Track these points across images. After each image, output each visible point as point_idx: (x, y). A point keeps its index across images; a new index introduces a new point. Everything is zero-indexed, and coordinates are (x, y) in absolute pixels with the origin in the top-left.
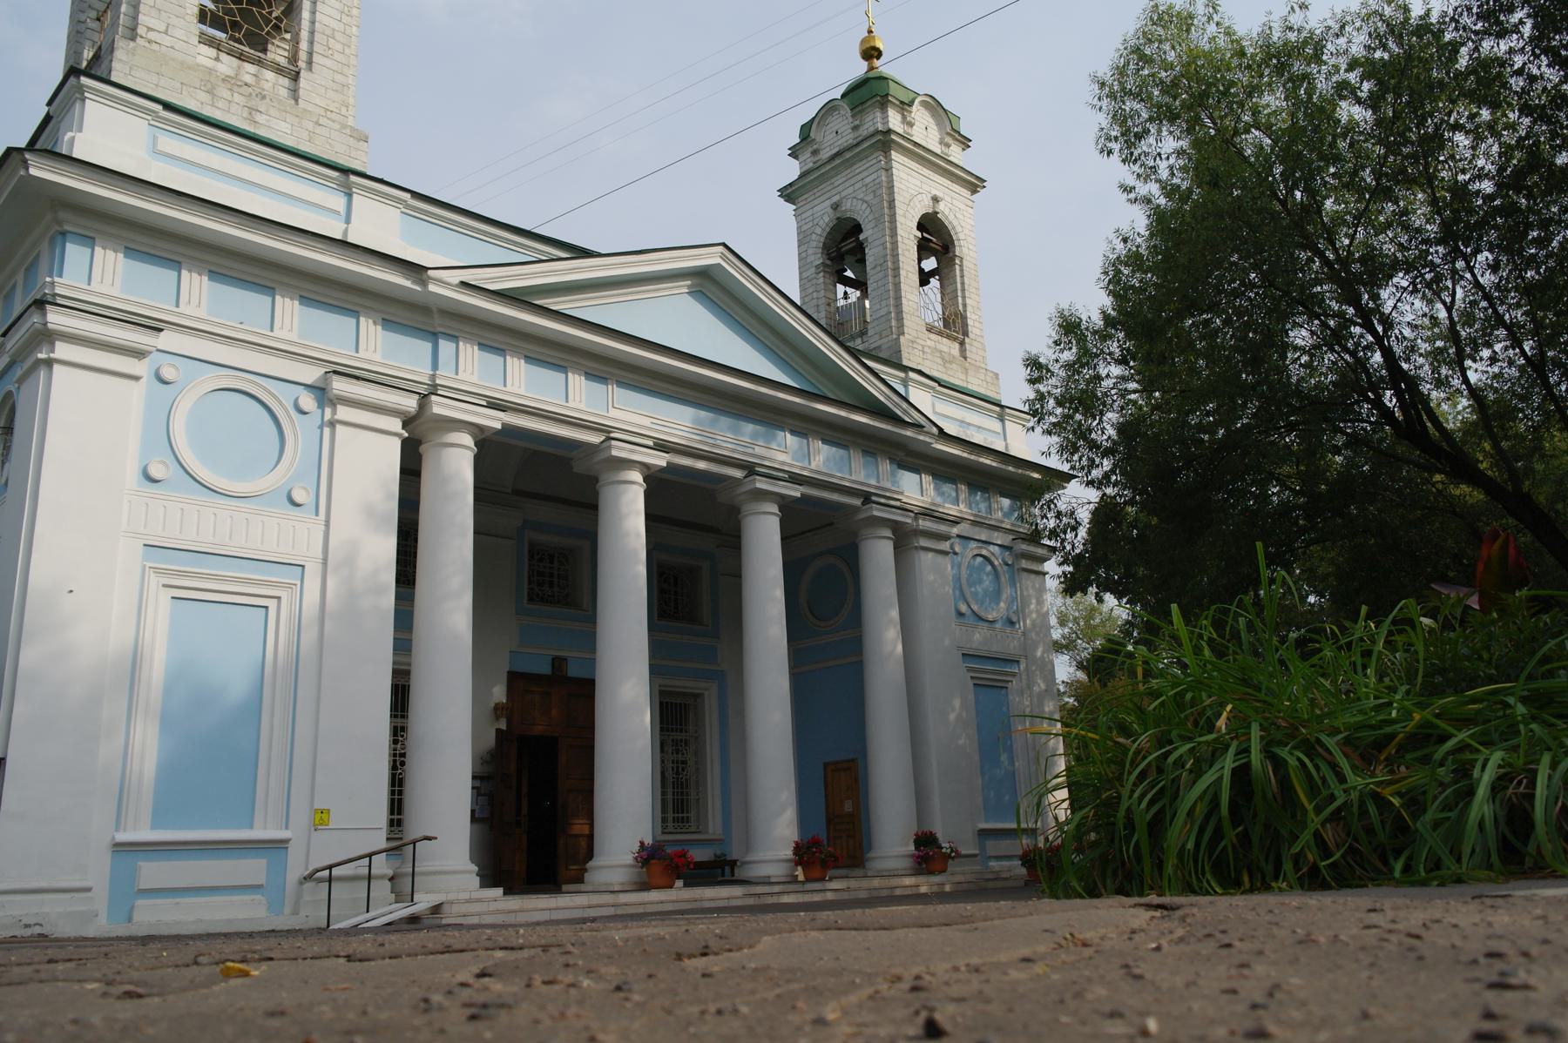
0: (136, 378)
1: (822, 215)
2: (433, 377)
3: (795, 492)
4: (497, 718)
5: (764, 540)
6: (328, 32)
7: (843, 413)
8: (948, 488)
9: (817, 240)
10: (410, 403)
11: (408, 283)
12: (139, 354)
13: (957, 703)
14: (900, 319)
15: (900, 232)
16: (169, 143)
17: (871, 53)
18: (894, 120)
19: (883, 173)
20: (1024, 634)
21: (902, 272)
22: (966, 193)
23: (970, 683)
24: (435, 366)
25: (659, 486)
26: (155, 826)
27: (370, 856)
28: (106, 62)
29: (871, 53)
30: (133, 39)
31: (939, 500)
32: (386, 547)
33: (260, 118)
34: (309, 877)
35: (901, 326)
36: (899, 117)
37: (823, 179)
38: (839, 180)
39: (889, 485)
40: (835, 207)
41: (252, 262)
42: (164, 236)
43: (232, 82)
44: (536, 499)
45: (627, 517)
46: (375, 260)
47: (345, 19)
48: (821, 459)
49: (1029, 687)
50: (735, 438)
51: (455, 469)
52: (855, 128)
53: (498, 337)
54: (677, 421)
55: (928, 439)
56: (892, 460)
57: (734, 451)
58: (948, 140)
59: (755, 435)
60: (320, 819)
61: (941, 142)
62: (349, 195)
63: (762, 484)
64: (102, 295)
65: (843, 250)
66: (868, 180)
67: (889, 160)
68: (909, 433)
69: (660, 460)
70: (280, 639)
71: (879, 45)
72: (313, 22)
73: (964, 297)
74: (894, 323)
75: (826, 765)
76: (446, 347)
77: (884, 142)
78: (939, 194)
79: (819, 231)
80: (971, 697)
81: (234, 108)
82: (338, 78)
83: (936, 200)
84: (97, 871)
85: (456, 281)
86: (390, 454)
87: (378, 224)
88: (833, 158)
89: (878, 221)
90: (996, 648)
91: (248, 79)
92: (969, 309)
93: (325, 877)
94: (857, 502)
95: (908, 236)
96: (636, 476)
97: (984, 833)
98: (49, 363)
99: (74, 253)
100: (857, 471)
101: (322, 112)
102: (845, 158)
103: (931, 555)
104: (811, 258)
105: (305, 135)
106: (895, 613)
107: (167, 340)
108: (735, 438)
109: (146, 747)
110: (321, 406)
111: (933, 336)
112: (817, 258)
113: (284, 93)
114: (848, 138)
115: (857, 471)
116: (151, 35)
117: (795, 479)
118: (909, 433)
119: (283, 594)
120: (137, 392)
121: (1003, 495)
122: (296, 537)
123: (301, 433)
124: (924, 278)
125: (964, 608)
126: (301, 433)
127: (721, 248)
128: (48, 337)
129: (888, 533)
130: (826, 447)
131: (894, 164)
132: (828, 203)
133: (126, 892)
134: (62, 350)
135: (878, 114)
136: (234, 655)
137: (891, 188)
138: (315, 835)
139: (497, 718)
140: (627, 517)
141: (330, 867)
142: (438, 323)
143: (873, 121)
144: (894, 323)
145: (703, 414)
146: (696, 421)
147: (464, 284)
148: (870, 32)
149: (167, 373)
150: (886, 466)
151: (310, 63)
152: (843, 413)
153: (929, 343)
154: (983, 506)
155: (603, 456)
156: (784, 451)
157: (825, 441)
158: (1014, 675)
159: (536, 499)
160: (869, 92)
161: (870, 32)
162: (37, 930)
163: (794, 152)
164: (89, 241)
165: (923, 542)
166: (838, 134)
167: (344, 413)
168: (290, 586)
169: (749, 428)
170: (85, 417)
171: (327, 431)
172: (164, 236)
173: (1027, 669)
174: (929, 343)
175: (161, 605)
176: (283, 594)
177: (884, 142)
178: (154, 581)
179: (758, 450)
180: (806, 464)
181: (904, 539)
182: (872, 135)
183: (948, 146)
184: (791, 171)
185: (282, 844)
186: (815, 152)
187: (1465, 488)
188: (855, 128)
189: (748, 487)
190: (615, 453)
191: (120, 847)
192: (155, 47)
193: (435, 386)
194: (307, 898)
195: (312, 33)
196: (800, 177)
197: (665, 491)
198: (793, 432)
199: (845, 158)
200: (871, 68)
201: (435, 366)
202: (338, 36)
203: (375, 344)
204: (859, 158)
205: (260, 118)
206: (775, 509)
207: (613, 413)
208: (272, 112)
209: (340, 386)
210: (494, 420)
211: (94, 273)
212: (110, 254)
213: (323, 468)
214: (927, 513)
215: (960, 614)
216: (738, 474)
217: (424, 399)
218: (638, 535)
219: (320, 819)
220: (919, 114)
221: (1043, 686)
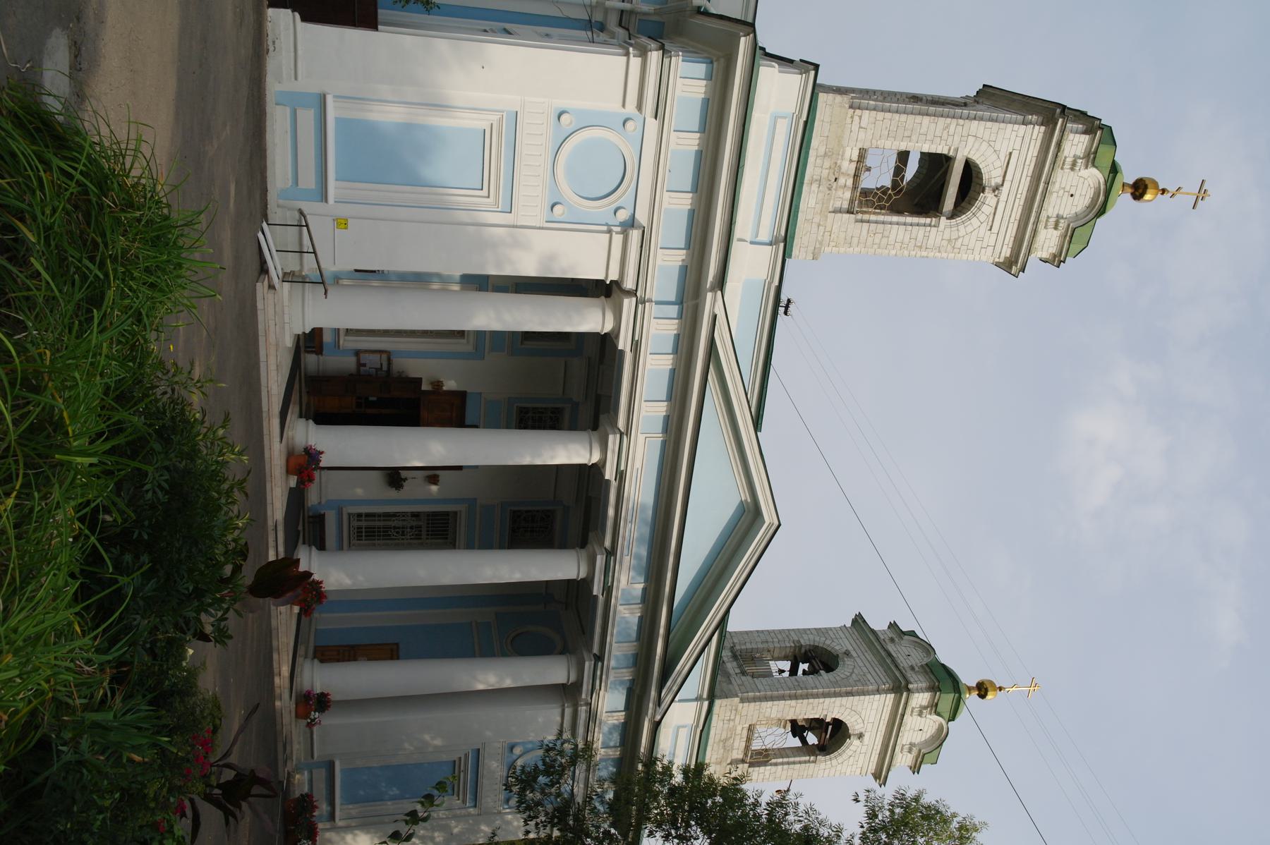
0: (624, 106)
1: (838, 646)
2: (650, 301)
3: (597, 589)
4: (432, 383)
5: (556, 566)
6: (886, 233)
7: (662, 631)
8: (616, 738)
9: (820, 641)
10: (629, 284)
11: (710, 278)
12: (640, 107)
13: (438, 742)
14: (755, 700)
15: (827, 700)
16: (783, 128)
17: (982, 689)
18: (921, 699)
19: (875, 687)
20: (500, 813)
21: (793, 702)
22: (872, 767)
23: (455, 758)
24: (658, 303)
25: (589, 476)
26: (338, 120)
27: (314, 252)
29: (982, 689)
30: (851, 107)
31: (605, 729)
32: (529, 268)
33: (815, 187)
34: (301, 213)
35: (749, 700)
36: (925, 703)
37: (870, 645)
38: (870, 656)
39: (611, 678)
40: (847, 653)
41: (714, 175)
42: (720, 126)
43: (836, 168)
44: (576, 380)
45: (567, 451)
46: (722, 255)
47: (898, 245)
48: (626, 615)
49: (455, 817)
50: (633, 536)
51: (588, 319)
52: (912, 668)
53: (684, 346)
54: (640, 490)
55: (650, 711)
56: (632, 681)
57: (624, 538)
58: (915, 751)
59: (638, 557)
60: (341, 223)
61: (912, 745)
62: (771, 244)
63: (600, 560)
64: (675, 84)
65: (815, 658)
66: (869, 676)
67: (887, 692)
68: (653, 693)
69: (609, 474)
70: (461, 198)
71: (989, 697)
72: (891, 223)
73: (782, 764)
74: (751, 694)
75: (397, 644)
76: (673, 310)
77: (900, 687)
78: (866, 738)
79: (828, 642)
80: (445, 758)
81: (818, 170)
82: (855, 240)
83: (860, 736)
84: (308, 84)
85: (717, 311)
86: (592, 271)
87: (750, 265)
88: (890, 655)
89: (835, 684)
90: (485, 783)
91: (842, 181)
92: (773, 768)
93: (302, 223)
94: (596, 650)
95: (829, 709)
96: (596, 458)
97: (330, 766)
98: (627, 54)
99: (700, 69)
100: (619, 649)
101: (828, 229)
102: (888, 662)
103: (559, 719)
104: (806, 637)
105: (809, 217)
106: (508, 683)
107: (652, 125)
108: (633, 536)
109: (389, 115)
110: (622, 224)
111: (745, 732)
112: (805, 641)
113: (838, 205)
114: (904, 663)
115: (619, 649)
116: (856, 118)
117: (608, 590)
118: (653, 693)
121: (616, 793)
122: (530, 207)
123: (601, 210)
124: (797, 729)
125: (517, 751)
126: (601, 210)
127: (776, 523)
128: (643, 53)
129: (573, 678)
130: (636, 620)
131: (883, 696)
132: (850, 648)
133: (295, 102)
134: (635, 62)
135: (924, 685)
136: (450, 170)
137: (863, 693)
138: (330, 219)
139: (432, 383)
140: (567, 451)
141: (307, 225)
142: (688, 304)
143: (918, 682)
144: (751, 694)
145: (650, 513)
146: (644, 507)
147: (715, 317)
148: (1000, 689)
149: (630, 125)
150: (627, 675)
151: (862, 221)
152: (662, 631)
153: (739, 728)
154: (604, 774)
155: (609, 429)
156: (628, 583)
157: (641, 618)
158: (464, 802)
159: (576, 380)
160: (943, 680)
161: (1000, 689)
162: (271, 48)
163: (893, 626)
164: (709, 77)
165: (568, 712)
166: (906, 656)
167: (617, 239)
169: (644, 552)
170: (595, 78)
171: (605, 228)
172: (720, 126)
173: (469, 815)
174: (739, 728)
175: (479, 122)
177: (900, 687)
178: (494, 118)
179: (626, 559)
180: (620, 602)
181: (569, 693)
182: (904, 677)
183: (910, 751)
184: (878, 623)
185: (324, 198)
186: (892, 640)
188: (912, 668)
189: (597, 551)
190: (611, 437)
191: (323, 98)
192: (849, 120)
193: (644, 302)
194: (288, 213)
195: (883, 223)
196: (873, 631)
197: (588, 482)
198: (644, 590)
199: (888, 662)
200: (970, 689)
201: (658, 303)
202: (885, 240)
203: (667, 262)
204: (887, 670)
205: (815, 187)
206: (583, 575)
207: (641, 438)
208: (821, 195)
209: (635, 235)
210: (624, 343)
211: (688, 81)
212: (703, 90)
213: (578, 225)
214: (592, 716)
215: (512, 748)
216: (608, 543)
217: (632, 293)
218: (552, 458)
219: (341, 223)
220: (931, 723)
221: (456, 831)
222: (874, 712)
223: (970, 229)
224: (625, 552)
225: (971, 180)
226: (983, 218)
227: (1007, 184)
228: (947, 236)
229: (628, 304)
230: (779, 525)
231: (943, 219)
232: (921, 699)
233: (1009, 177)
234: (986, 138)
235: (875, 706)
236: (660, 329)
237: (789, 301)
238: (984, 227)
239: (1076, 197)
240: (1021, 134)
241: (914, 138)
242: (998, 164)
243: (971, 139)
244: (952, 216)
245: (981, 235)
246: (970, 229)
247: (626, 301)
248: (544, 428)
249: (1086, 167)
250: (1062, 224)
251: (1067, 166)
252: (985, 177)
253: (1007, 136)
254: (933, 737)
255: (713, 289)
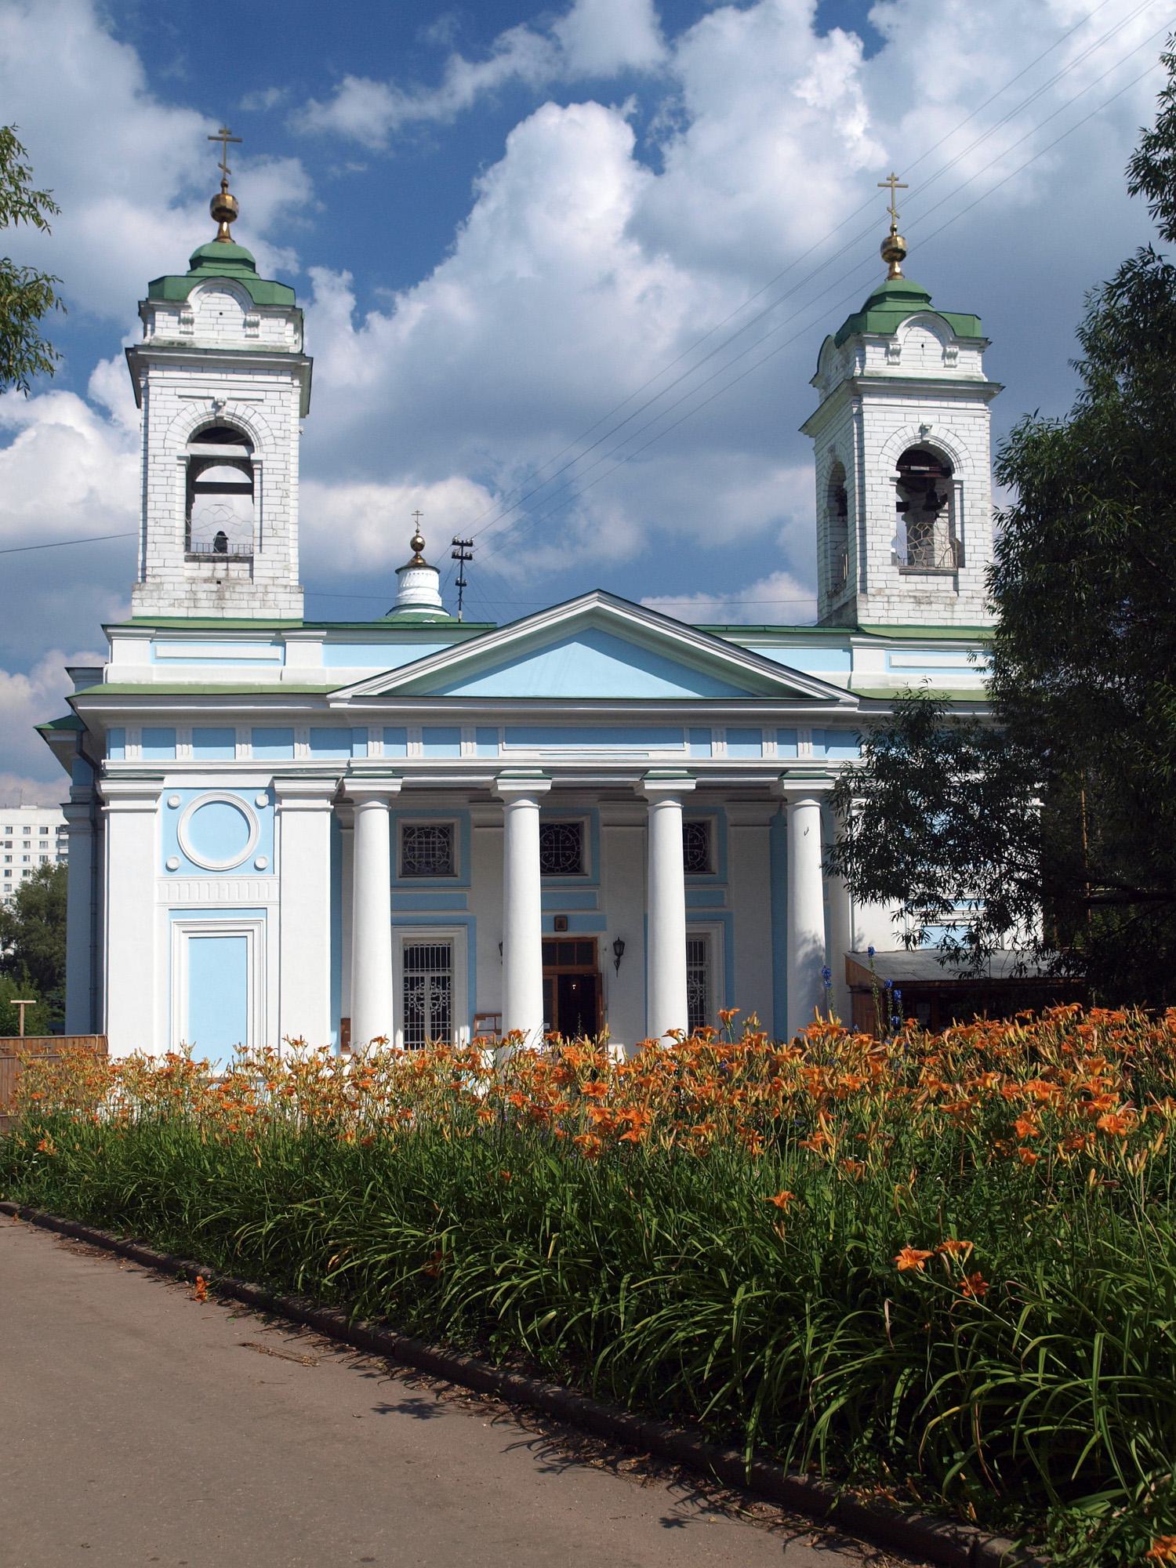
0: (154, 811)
10: (331, 786)
12: (154, 796)
28: (823, 487)
40: (923, 430)
41: (213, 718)
51: (376, 830)
77: (856, 389)
86: (323, 823)
91: (220, 574)
107: (170, 781)
116: (156, 571)
119: (256, 928)
120: (156, 820)
134: (113, 805)
149: (173, 803)
167: (286, 803)
168: (258, 922)
176: (256, 928)
178: (177, 929)
187: (114, 1239)
193: (350, 770)
203: (302, 754)
209: (280, 786)
213: (275, 843)
222: (889, 416)
224: (644, 757)
226: (250, 412)
227: (212, 393)
228: (272, 448)
229: (351, 786)
231: (253, 457)
233: (204, 393)
234: (164, 428)
235: (881, 416)
236: (376, 752)
237: (455, 543)
239: (221, 308)
240: (159, 390)
241: (169, 506)
242: (191, 408)
243: (168, 444)
244: (248, 443)
245: (268, 410)
246: (262, 424)
247: (348, 788)
249: (189, 307)
250: (253, 318)
251: (189, 328)
252: (206, 419)
253: (161, 405)
254: (931, 329)
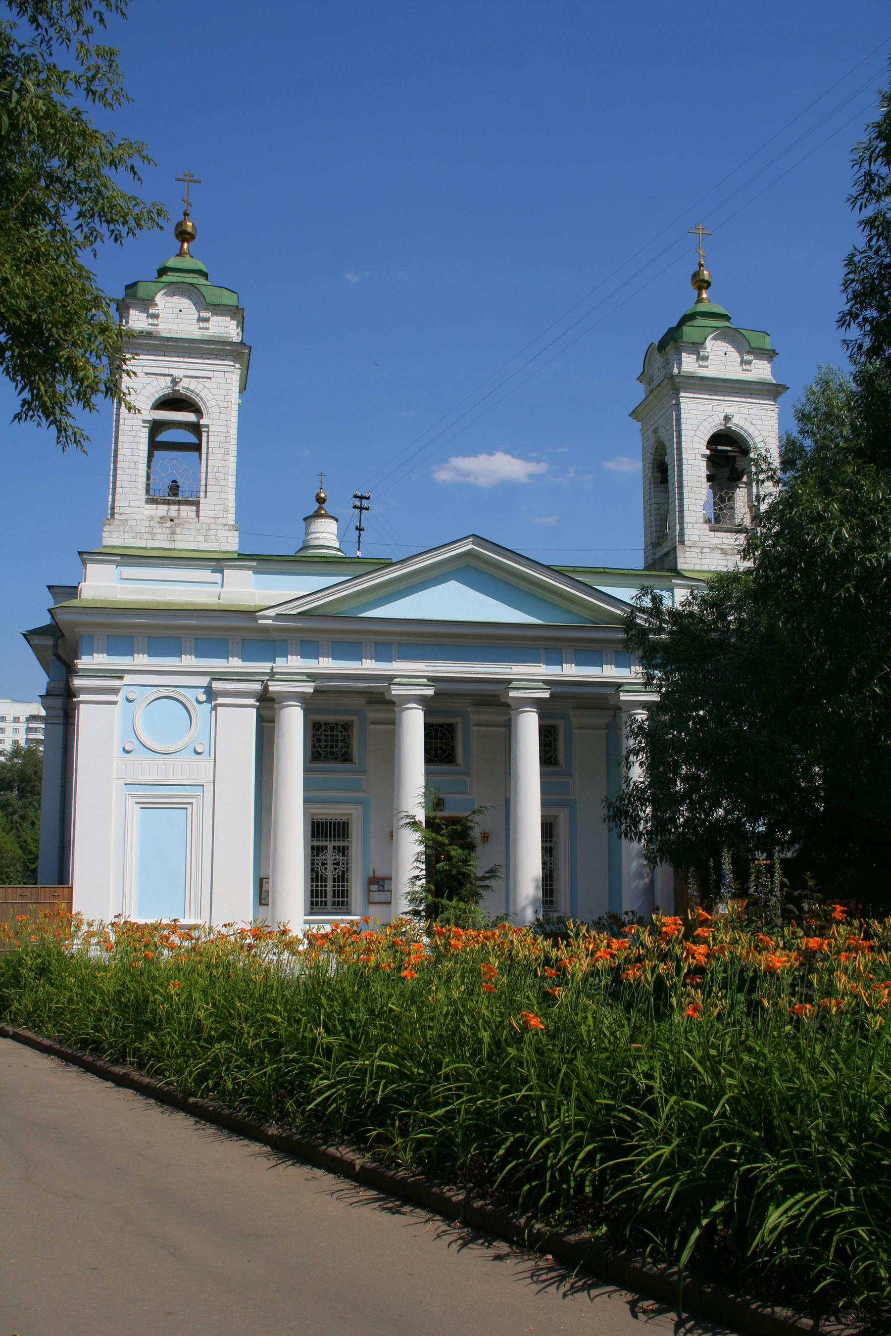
10: (257, 687)
40: (727, 418)
51: (293, 723)
61: (743, 362)
67: (677, 398)
91: (173, 514)
107: (128, 679)
116: (122, 510)
167: (220, 700)
209: (216, 685)
222: (701, 407)
223: (210, 397)
225: (174, 401)
226: (200, 387)
227: (171, 372)
228: (217, 416)
229: (274, 687)
230: (474, 535)
231: (202, 422)
232: (689, 364)
233: (165, 371)
238: (208, 384)
242: (155, 383)
246: (210, 397)
247: (271, 689)
248: (310, 746)
249: (156, 305)
252: (166, 391)
255: (256, 619)
